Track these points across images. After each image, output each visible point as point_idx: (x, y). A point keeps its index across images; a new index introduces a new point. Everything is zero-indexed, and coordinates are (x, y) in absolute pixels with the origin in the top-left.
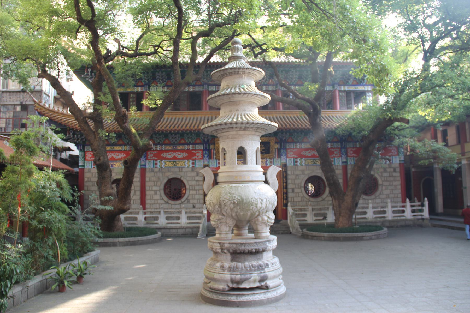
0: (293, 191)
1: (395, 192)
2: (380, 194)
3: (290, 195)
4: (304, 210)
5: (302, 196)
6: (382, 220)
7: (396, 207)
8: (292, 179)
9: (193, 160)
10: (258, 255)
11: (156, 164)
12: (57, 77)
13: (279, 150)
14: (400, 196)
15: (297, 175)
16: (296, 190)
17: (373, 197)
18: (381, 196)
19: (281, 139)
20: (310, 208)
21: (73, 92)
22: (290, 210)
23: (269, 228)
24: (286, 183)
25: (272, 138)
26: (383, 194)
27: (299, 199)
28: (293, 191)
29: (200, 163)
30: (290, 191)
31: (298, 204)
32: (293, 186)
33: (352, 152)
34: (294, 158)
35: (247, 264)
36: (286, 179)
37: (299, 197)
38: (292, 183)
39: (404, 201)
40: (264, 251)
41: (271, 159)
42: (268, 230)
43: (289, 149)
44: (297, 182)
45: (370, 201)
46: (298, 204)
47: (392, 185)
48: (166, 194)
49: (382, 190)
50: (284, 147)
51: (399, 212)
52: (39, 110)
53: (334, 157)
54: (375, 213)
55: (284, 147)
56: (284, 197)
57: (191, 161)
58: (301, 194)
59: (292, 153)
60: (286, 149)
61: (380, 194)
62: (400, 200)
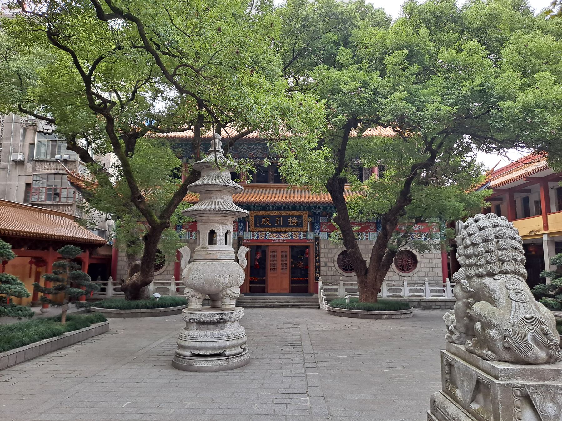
0: (326, 265)
1: (435, 270)
2: (419, 271)
3: (322, 269)
4: (337, 285)
5: (335, 270)
6: (418, 299)
7: (436, 285)
8: (325, 253)
9: (367, 232)
10: (220, 325)
11: (191, 235)
12: (86, 149)
13: (313, 224)
14: (441, 274)
15: (330, 249)
16: (329, 264)
17: (410, 274)
18: (419, 274)
19: (315, 213)
20: (341, 283)
21: (482, 164)
22: (320, 283)
23: (235, 301)
24: (319, 256)
25: (305, 212)
26: (421, 271)
27: (332, 273)
28: (326, 265)
29: (373, 235)
30: (322, 264)
31: (330, 279)
32: (327, 260)
33: (326, 227)
34: (327, 231)
35: (209, 333)
36: (319, 253)
37: (331, 271)
38: (325, 257)
39: (444, 281)
40: (225, 321)
41: (304, 232)
42: (234, 302)
43: (322, 222)
44: (330, 255)
45: (405, 278)
46: (330, 279)
47: (432, 263)
48: (340, 266)
49: (420, 267)
50: (317, 220)
51: (439, 291)
52: (72, 181)
53: (370, 232)
54: (432, 291)
55: (317, 220)
56: (316, 270)
57: (365, 234)
58: (334, 268)
59: (326, 227)
60: (320, 222)
61: (419, 271)
62: (441, 278)
